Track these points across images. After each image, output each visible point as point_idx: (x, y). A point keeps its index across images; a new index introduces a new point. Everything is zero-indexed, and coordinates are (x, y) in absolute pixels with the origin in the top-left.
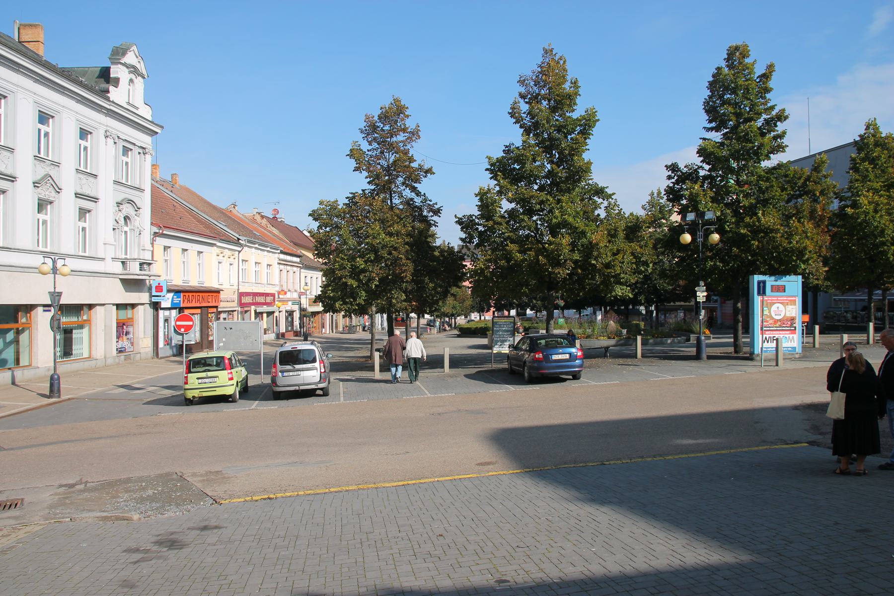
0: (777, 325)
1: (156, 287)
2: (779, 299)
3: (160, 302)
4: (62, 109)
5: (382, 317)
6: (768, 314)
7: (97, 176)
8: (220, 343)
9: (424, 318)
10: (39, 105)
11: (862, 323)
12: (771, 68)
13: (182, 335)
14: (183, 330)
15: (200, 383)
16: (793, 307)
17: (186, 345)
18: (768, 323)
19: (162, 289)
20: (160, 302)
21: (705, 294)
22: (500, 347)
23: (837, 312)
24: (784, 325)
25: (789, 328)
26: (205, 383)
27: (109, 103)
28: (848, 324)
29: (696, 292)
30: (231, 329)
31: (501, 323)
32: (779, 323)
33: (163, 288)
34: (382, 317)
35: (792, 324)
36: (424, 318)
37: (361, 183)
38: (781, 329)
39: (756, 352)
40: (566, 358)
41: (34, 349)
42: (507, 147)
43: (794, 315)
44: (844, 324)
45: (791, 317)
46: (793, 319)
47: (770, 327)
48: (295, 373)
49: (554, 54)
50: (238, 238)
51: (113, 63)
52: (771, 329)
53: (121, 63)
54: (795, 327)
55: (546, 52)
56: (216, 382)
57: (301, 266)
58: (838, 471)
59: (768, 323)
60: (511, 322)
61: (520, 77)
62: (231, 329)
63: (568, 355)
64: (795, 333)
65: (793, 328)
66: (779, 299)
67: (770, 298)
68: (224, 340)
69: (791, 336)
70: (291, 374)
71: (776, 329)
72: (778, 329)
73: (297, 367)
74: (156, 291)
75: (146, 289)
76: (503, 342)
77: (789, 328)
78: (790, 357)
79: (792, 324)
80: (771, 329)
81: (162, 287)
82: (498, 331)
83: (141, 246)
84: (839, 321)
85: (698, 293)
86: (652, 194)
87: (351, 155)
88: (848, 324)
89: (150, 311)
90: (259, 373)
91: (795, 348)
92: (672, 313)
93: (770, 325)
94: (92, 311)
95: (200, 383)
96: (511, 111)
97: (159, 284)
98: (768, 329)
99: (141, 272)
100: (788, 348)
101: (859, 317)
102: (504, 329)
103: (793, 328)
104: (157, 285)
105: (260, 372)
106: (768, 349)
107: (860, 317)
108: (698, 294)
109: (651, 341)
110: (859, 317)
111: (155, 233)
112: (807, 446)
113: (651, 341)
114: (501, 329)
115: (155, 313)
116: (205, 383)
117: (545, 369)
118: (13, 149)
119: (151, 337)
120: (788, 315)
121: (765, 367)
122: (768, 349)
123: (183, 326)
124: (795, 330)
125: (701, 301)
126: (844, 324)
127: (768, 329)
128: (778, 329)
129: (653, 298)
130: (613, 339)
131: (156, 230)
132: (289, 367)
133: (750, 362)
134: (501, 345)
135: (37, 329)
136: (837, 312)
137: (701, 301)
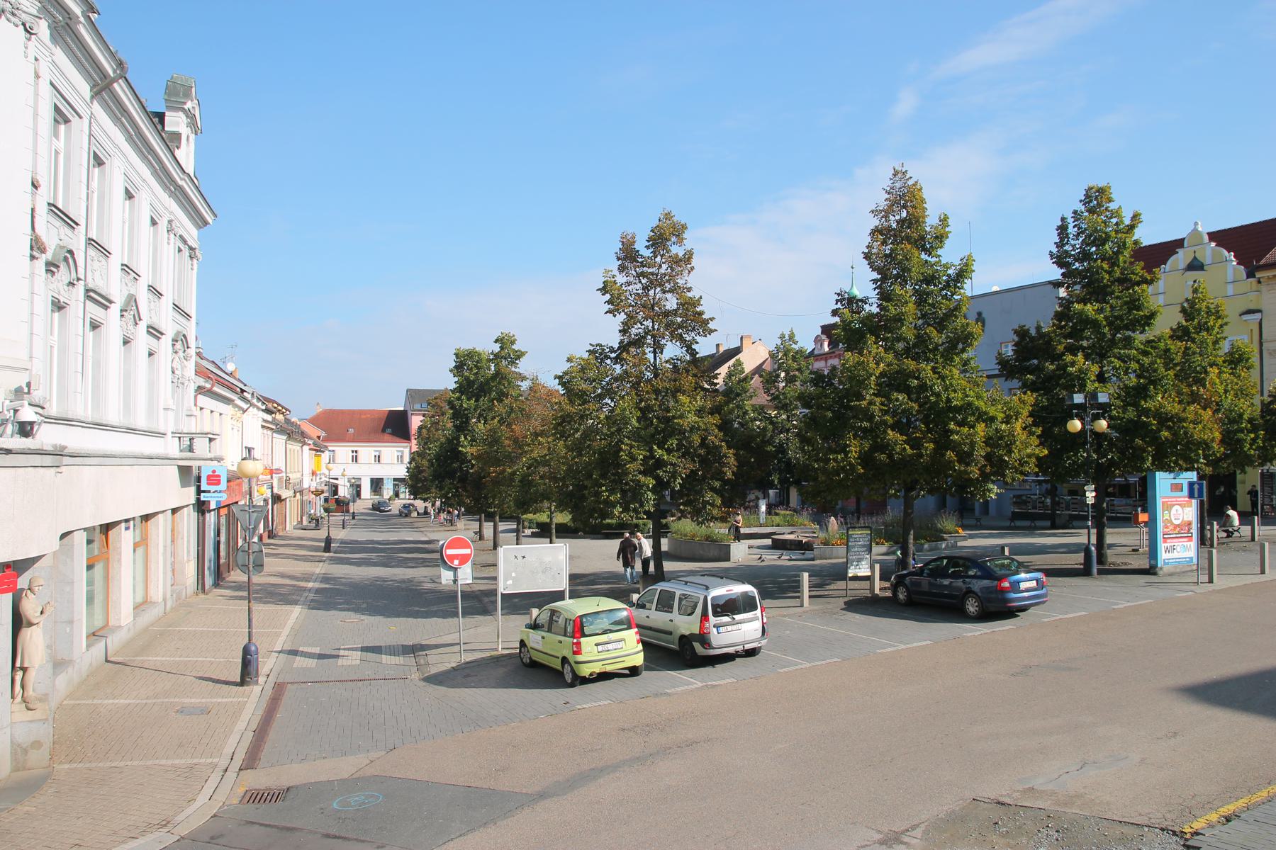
0: (1176, 532)
1: (209, 477)
2: (1178, 499)
3: (209, 501)
4: (142, 183)
5: (1081, 564)
7: (161, 295)
8: (507, 581)
9: (360, 499)
10: (128, 180)
12: (1136, 217)
13: (455, 569)
14: (456, 562)
15: (601, 652)
18: (1168, 530)
19: (219, 481)
20: (209, 501)
21: (1094, 494)
22: (855, 569)
23: (1032, 497)
24: (1183, 532)
25: (1186, 535)
26: (608, 651)
27: (182, 176)
28: (1081, 513)
29: (1085, 491)
30: (524, 557)
31: (857, 536)
33: (221, 478)
34: (1081, 564)
35: (1189, 530)
36: (360, 499)
37: (609, 332)
38: (1179, 535)
39: (1159, 565)
40: (1032, 586)
41: (113, 597)
42: (838, 295)
43: (1190, 519)
45: (1188, 521)
46: (1190, 524)
47: (1170, 534)
48: (735, 627)
50: (241, 389)
51: (170, 108)
52: (1172, 536)
53: (183, 110)
54: (1192, 533)
56: (622, 648)
57: (274, 427)
59: (1168, 530)
60: (867, 534)
62: (524, 557)
63: (1035, 582)
64: (1192, 541)
65: (1190, 535)
66: (1178, 499)
67: (1170, 500)
68: (513, 575)
69: (1189, 543)
70: (729, 628)
71: (1174, 536)
72: (1178, 536)
73: (738, 617)
74: (209, 484)
75: (193, 480)
76: (859, 560)
77: (1186, 535)
79: (1189, 530)
81: (219, 476)
82: (854, 546)
83: (185, 408)
84: (1035, 508)
85: (1087, 493)
86: (782, 337)
87: (604, 290)
88: (1081, 513)
89: (194, 515)
90: (455, 615)
91: (1191, 558)
92: (752, 492)
93: (1170, 532)
94: (149, 522)
95: (601, 652)
96: (867, 251)
97: (214, 471)
98: (1169, 536)
99: (181, 453)
100: (1185, 558)
101: (1062, 503)
102: (860, 543)
103: (1190, 535)
104: (211, 474)
105: (458, 613)
108: (1088, 494)
109: (926, 546)
110: (1062, 503)
111: (200, 388)
114: (856, 543)
115: (201, 518)
116: (608, 651)
118: (110, 253)
119: (194, 558)
120: (1186, 519)
123: (456, 557)
125: (1090, 503)
127: (1169, 536)
128: (1178, 536)
129: (789, 478)
131: (201, 382)
132: (726, 619)
133: (1152, 576)
134: (857, 565)
135: (120, 560)
136: (1032, 497)
137: (1090, 503)
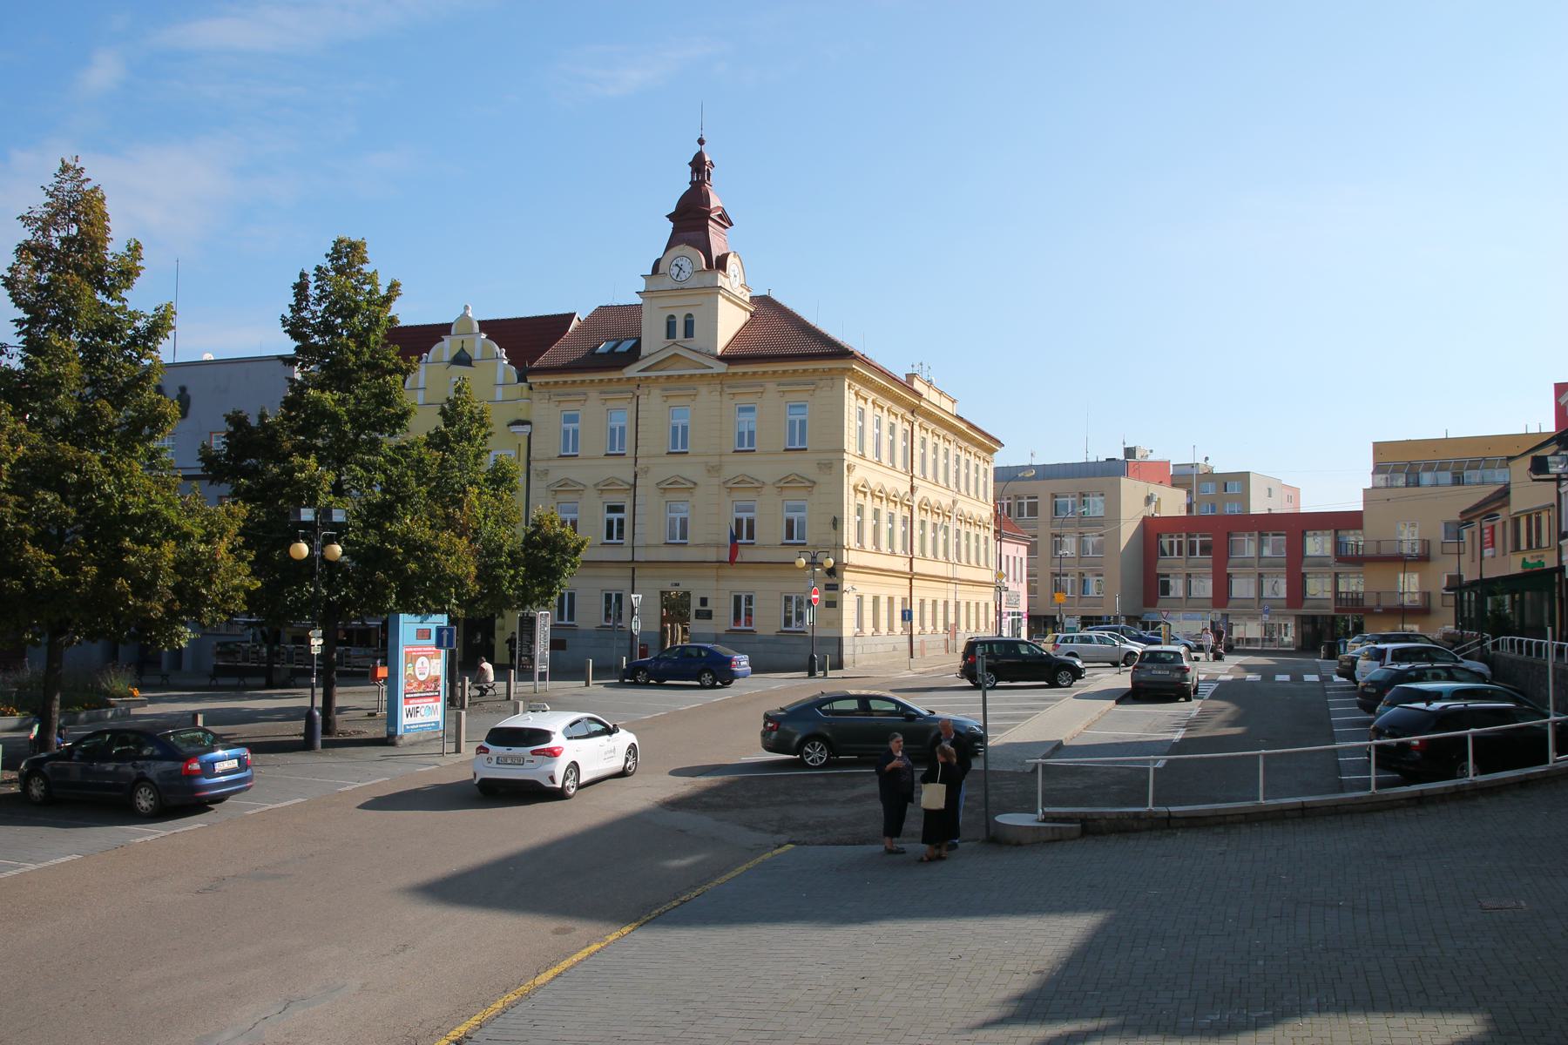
5: (301, 735)
6: (413, 673)
11: (288, 662)
16: (439, 661)
17: (1154, 806)
23: (243, 645)
24: (428, 690)
29: (310, 638)
32: (423, 686)
35: (436, 688)
38: (424, 694)
43: (438, 674)
44: (255, 665)
47: (413, 693)
49: (82, 178)
52: (415, 695)
54: (439, 692)
55: (65, 169)
58: (925, 859)
61: (30, 210)
67: (415, 649)
69: (435, 704)
78: (435, 736)
79: (436, 688)
80: (415, 695)
84: (246, 660)
85: (313, 640)
88: (355, 669)
93: (414, 691)
98: (412, 696)
101: (283, 654)
103: (437, 694)
106: (412, 727)
107: (286, 652)
109: (82, 716)
112: (792, 849)
113: (82, 716)
117: (206, 790)
121: (448, 755)
122: (412, 727)
124: (439, 695)
125: (316, 653)
126: (255, 665)
127: (412, 696)
130: (11, 715)
137: (316, 653)
